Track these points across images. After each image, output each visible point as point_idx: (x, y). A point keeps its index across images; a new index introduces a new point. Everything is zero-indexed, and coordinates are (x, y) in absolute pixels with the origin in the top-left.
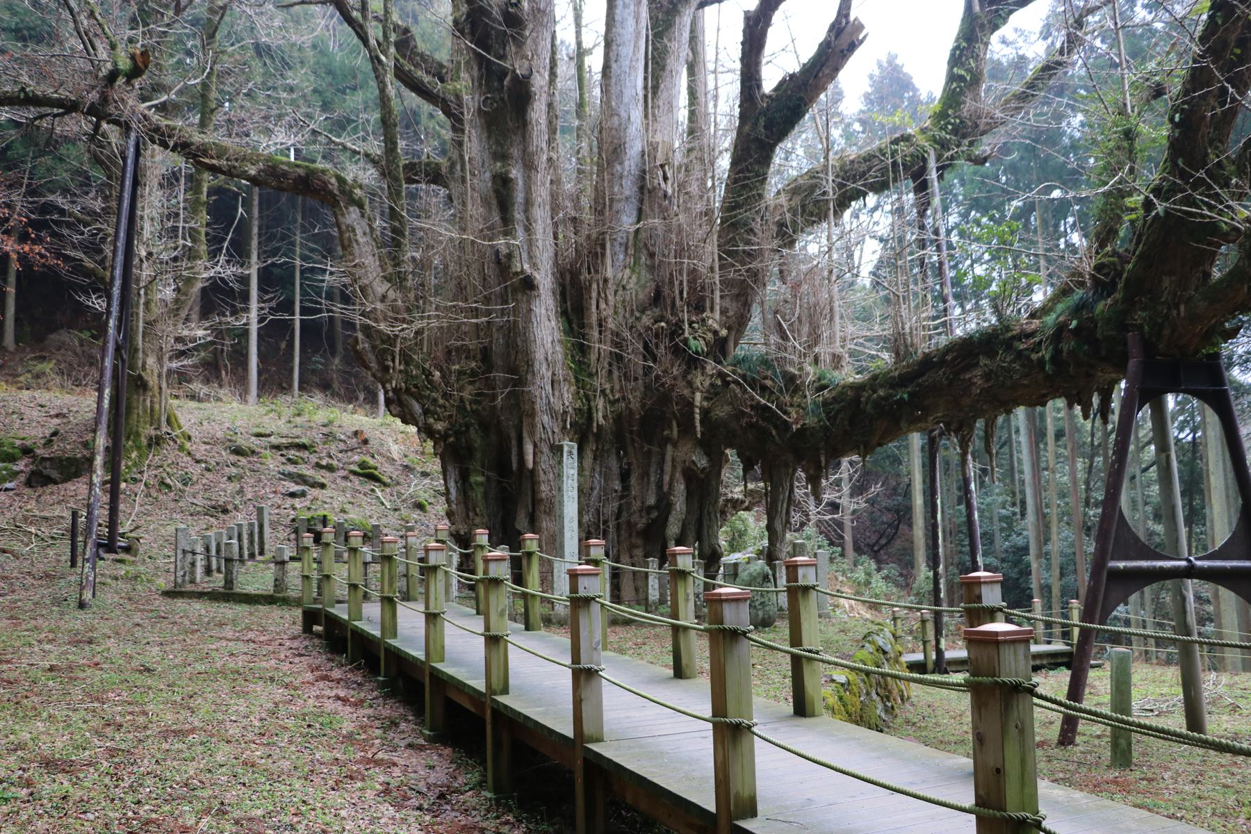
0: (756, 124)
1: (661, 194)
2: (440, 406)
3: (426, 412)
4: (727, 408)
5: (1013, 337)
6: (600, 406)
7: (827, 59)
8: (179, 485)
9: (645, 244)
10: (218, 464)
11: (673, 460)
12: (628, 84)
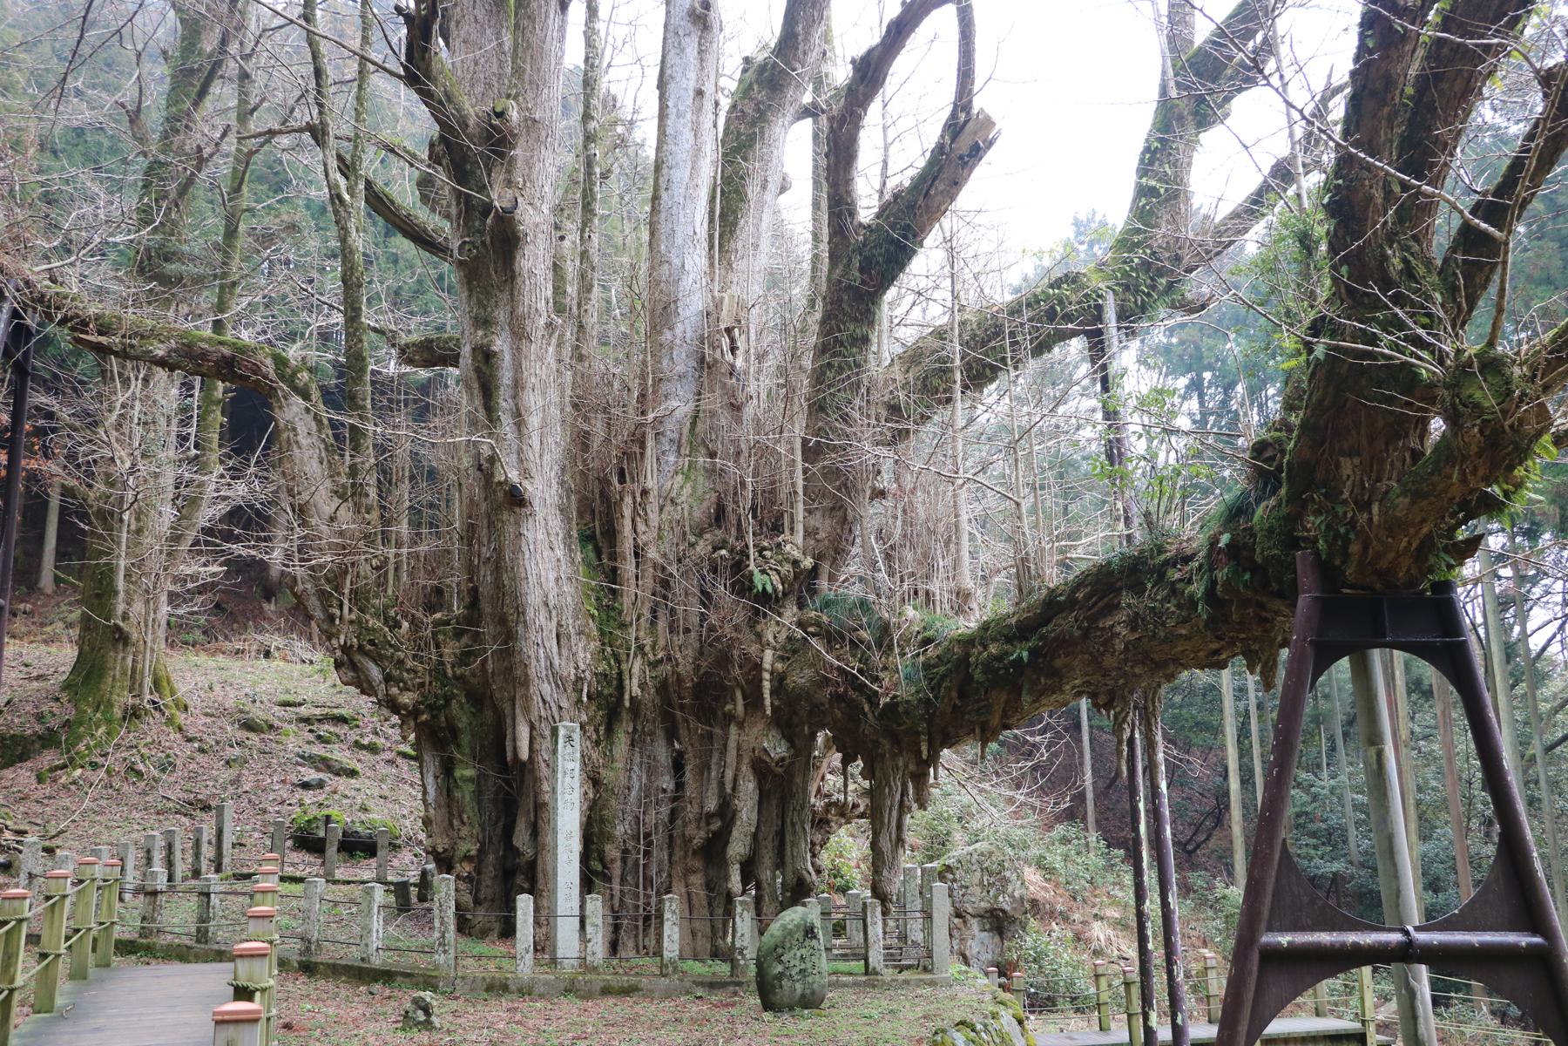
0: (848, 266)
1: (725, 369)
2: (408, 671)
3: (388, 679)
4: (808, 672)
5: (1166, 563)
7: (939, 171)
8: (156, 773)
9: (703, 441)
10: (218, 743)
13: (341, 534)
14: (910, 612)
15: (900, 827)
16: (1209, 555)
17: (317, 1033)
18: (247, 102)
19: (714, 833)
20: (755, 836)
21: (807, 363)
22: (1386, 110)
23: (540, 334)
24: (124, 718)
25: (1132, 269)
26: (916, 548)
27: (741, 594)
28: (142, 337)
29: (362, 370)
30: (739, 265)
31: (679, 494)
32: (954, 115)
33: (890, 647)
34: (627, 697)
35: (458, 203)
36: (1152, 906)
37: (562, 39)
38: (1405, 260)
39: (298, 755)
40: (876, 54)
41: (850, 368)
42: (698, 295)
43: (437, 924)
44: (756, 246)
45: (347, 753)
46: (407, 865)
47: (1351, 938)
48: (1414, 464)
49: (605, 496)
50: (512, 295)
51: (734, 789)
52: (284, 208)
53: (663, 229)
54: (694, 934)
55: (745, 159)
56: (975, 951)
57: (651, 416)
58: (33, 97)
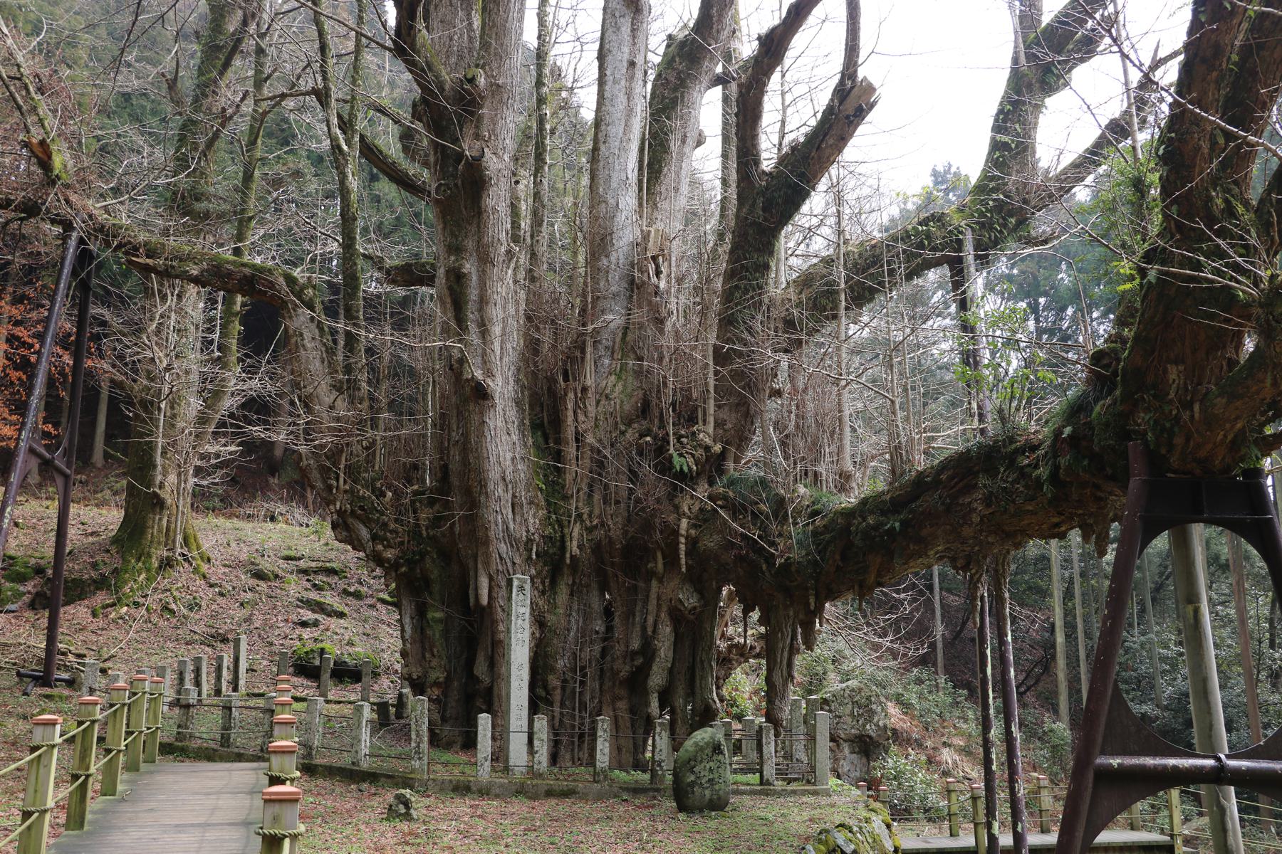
0: (753, 205)
2: (391, 532)
3: (374, 538)
6: (575, 534)
7: (830, 128)
8: (185, 611)
11: (659, 598)
12: (617, 167)
13: (338, 420)
14: (802, 490)
15: (790, 665)
16: (1053, 445)
17: (319, 821)
18: (262, 72)
19: (637, 668)
20: (671, 671)
21: (718, 284)
22: (1215, 74)
23: (501, 259)
24: (160, 567)
25: (987, 210)
26: (808, 440)
27: (662, 472)
28: (181, 260)
29: (356, 288)
30: (663, 205)
31: (612, 391)
32: (842, 82)
33: (785, 517)
34: (568, 555)
35: (436, 153)
36: (995, 733)
37: (521, 20)
38: (1226, 201)
40: (778, 31)
41: (754, 290)
42: (630, 228)
43: (413, 736)
44: (676, 190)
45: (337, 599)
46: (387, 688)
47: (1172, 762)
48: (1230, 371)
49: (552, 393)
50: (479, 227)
51: (654, 632)
52: (290, 158)
53: (602, 175)
54: (619, 749)
55: (668, 118)
56: (846, 769)
57: (590, 328)
58: (94, 68)
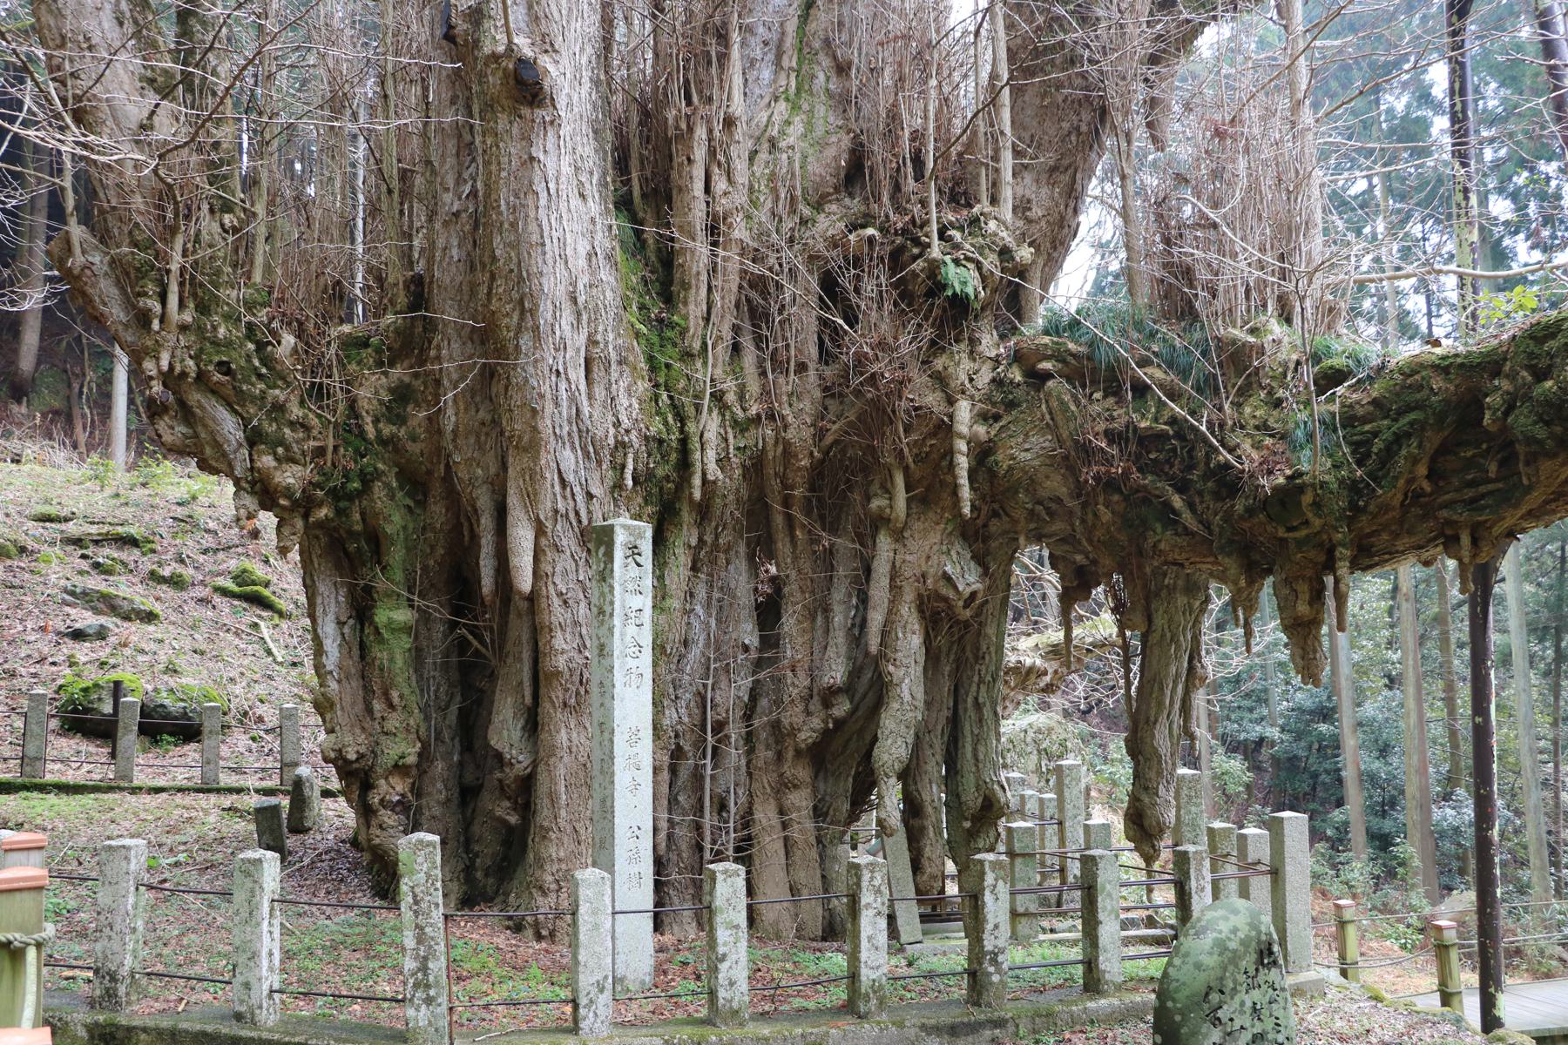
2: (292, 424)
3: (254, 439)
6: (712, 434)
9: (827, 42)
11: (894, 574)
19: (840, 723)
31: (782, 133)
39: (66, 591)
45: (140, 588)
